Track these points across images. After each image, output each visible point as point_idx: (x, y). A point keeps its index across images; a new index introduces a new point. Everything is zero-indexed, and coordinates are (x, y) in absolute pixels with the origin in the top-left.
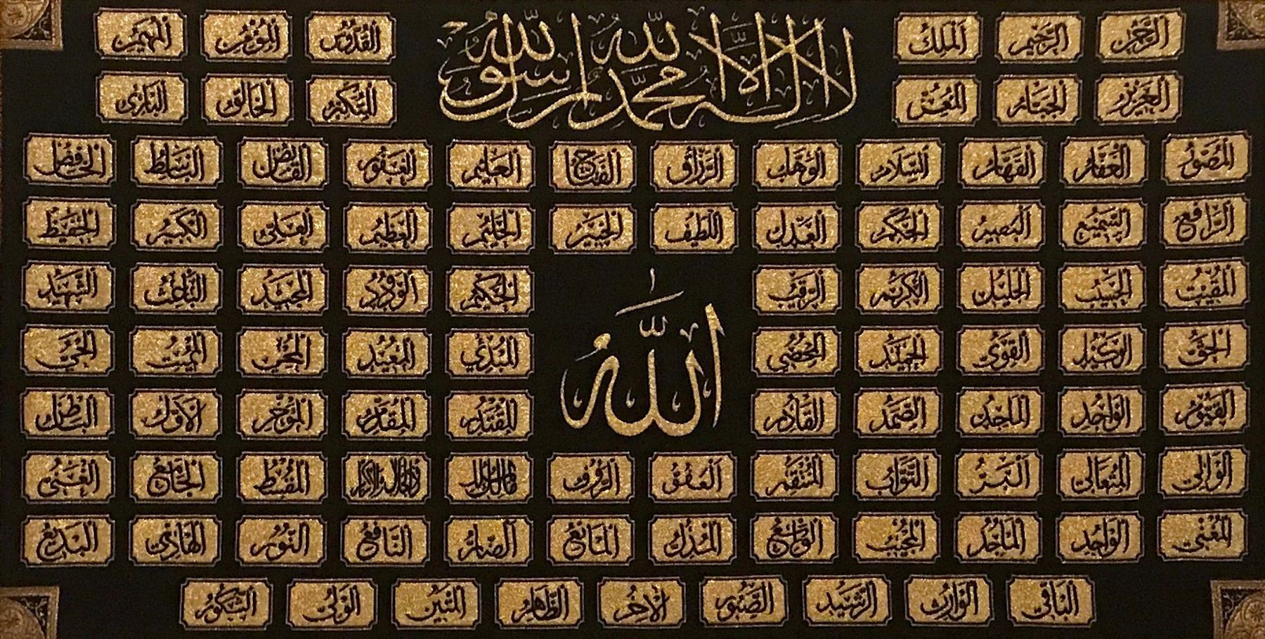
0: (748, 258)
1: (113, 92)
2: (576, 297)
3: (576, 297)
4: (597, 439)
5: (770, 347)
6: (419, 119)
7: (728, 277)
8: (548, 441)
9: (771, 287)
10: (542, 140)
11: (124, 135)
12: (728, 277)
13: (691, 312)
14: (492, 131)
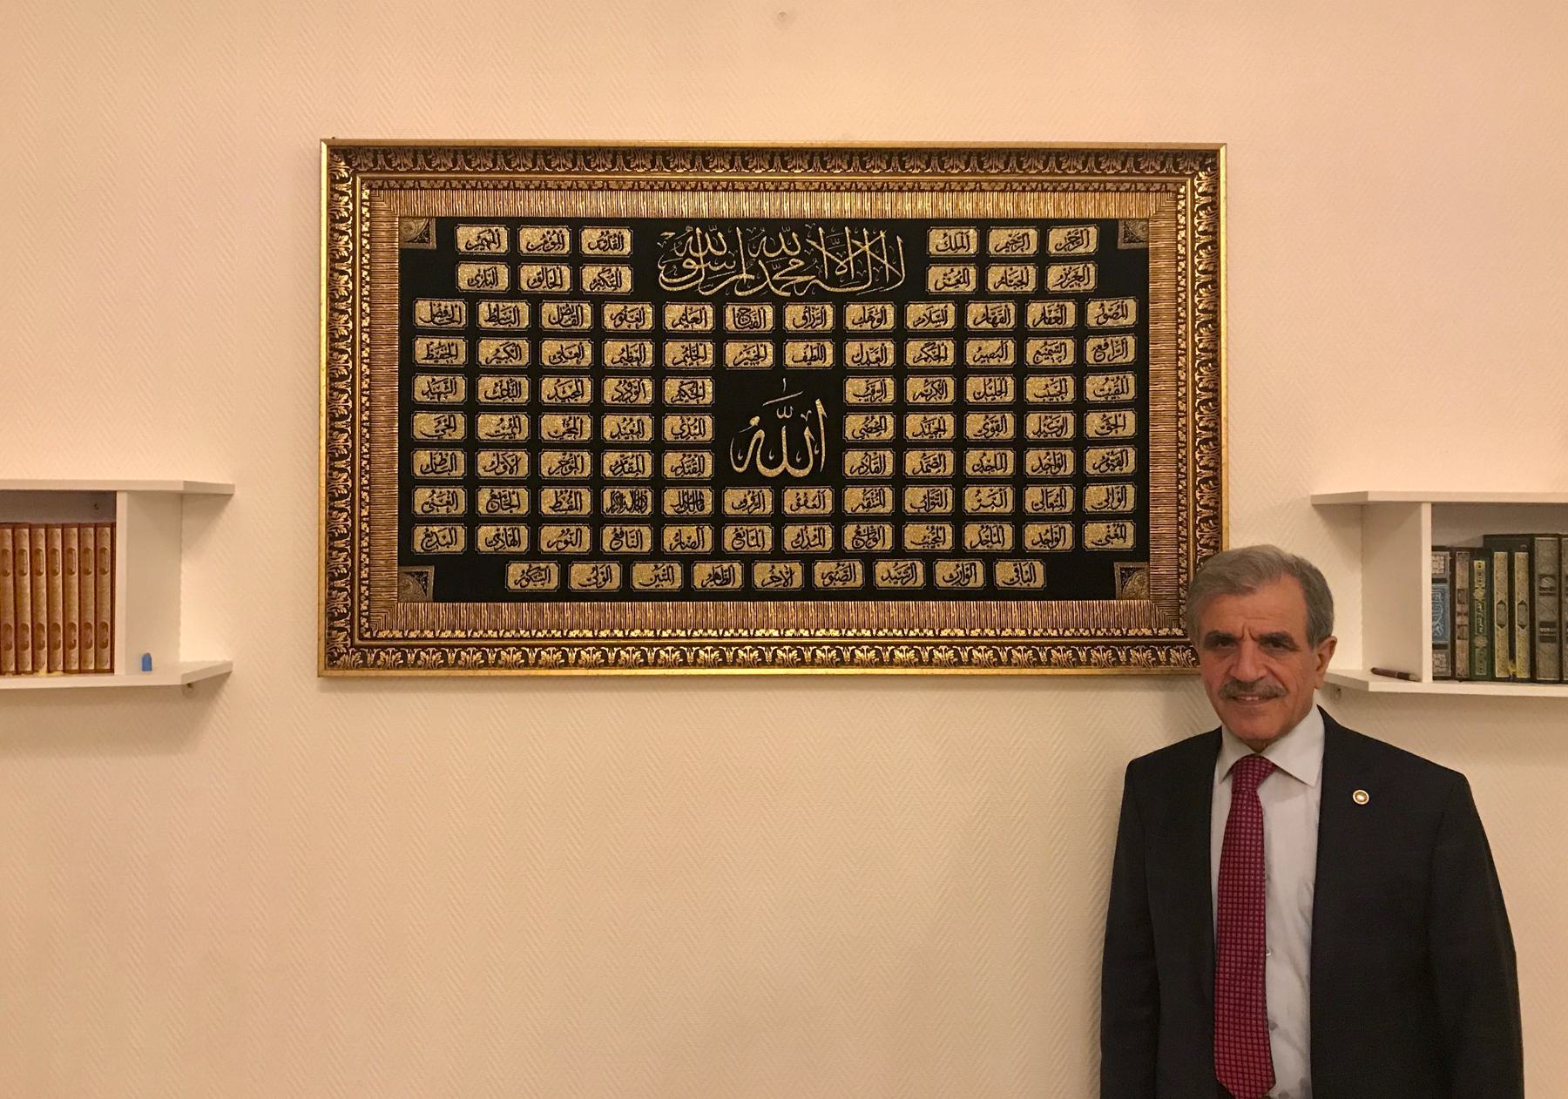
0: (841, 372)
1: (466, 273)
2: (739, 394)
3: (739, 394)
4: (752, 479)
5: (854, 425)
6: (646, 289)
7: (829, 383)
8: (723, 480)
9: (855, 389)
10: (719, 303)
11: (473, 299)
12: (829, 383)
13: (806, 403)
14: (690, 297)
